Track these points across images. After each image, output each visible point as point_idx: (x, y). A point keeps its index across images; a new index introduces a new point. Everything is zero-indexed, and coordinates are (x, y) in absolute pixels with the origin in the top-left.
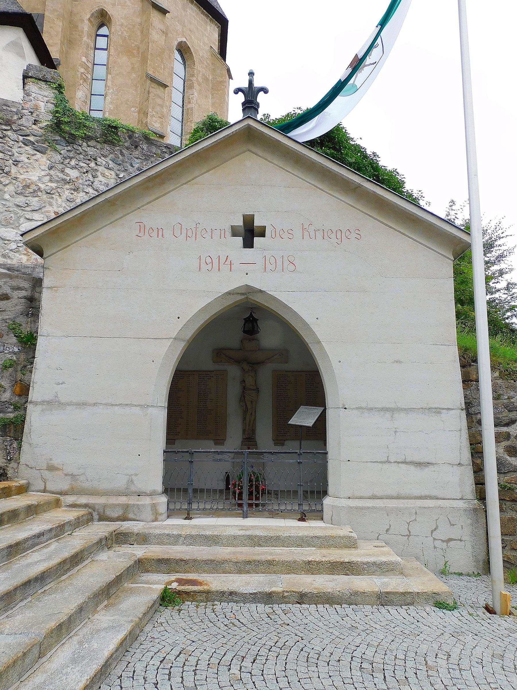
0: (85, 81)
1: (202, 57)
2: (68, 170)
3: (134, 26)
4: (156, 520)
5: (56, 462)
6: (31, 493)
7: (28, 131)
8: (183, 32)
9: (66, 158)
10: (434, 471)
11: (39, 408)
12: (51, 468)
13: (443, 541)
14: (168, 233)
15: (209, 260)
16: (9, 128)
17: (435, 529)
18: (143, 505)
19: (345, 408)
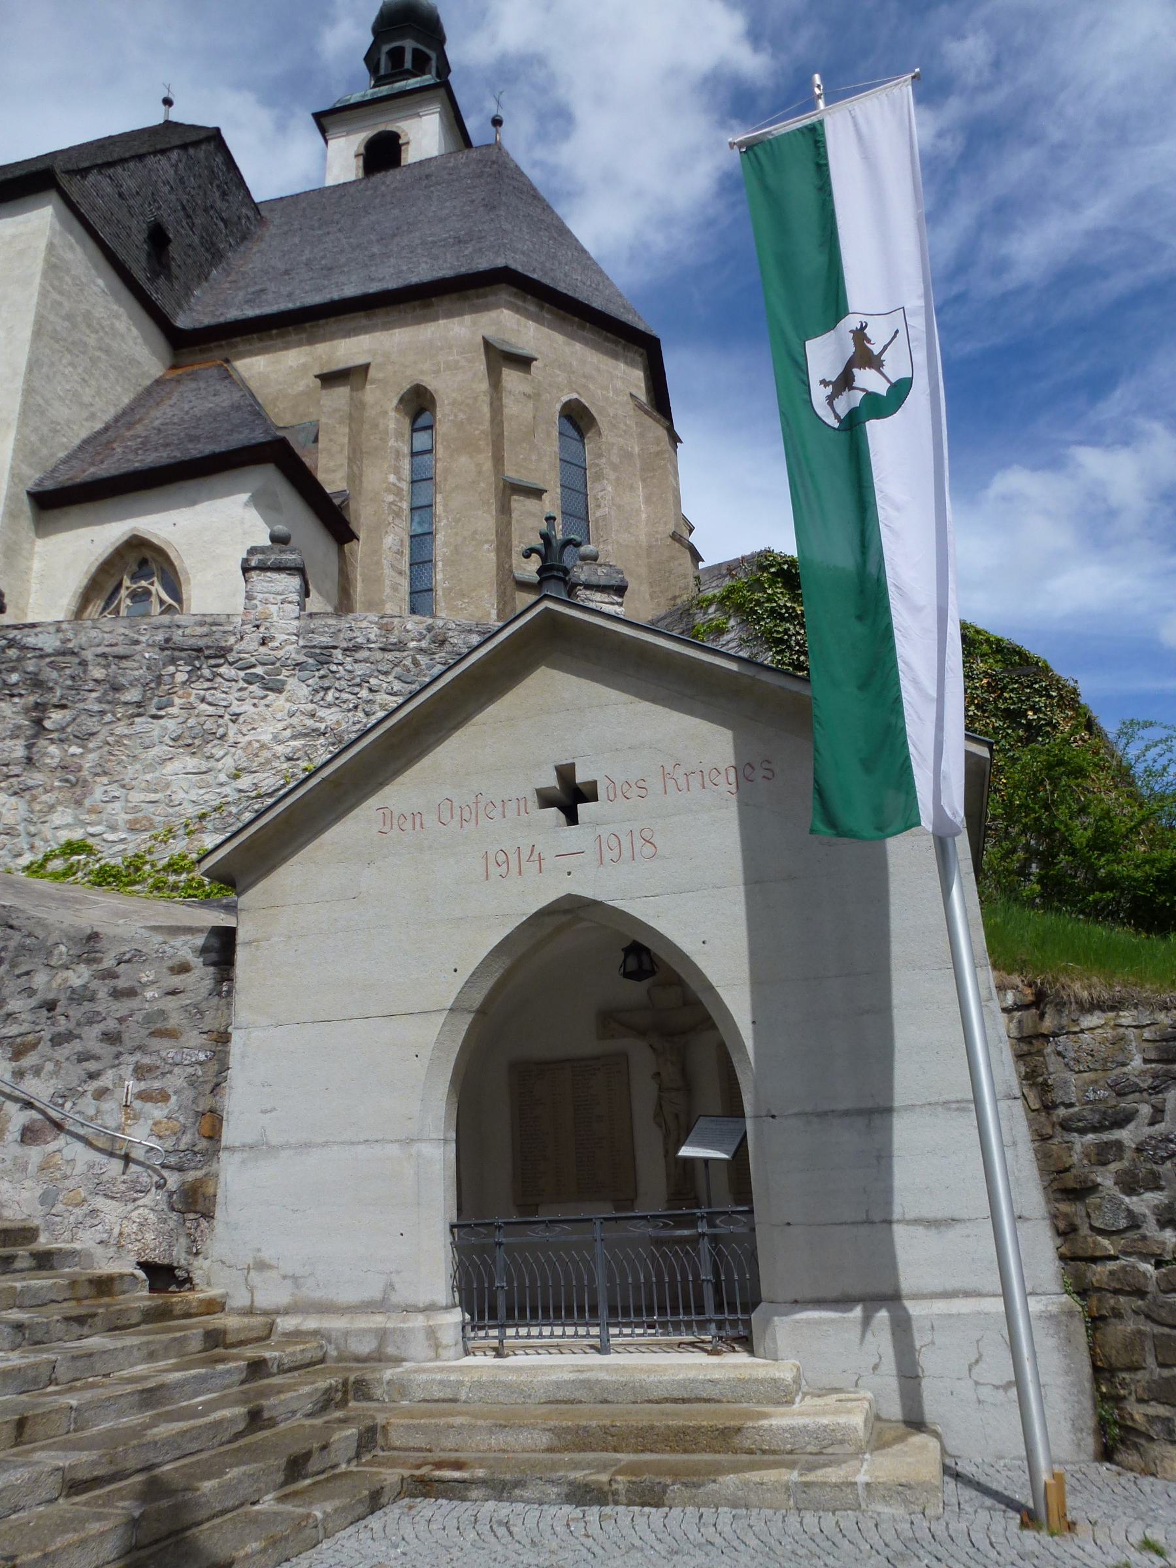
0: (398, 515)
1: (615, 416)
2: (322, 713)
3: (476, 398)
4: (437, 1357)
5: (267, 1255)
6: (122, 1297)
7: (253, 660)
8: (570, 382)
9: (317, 691)
10: (968, 1236)
11: (237, 1157)
12: (262, 1266)
13: (997, 1387)
14: (430, 820)
15: (501, 858)
16: (222, 661)
17: (977, 1361)
18: (411, 1330)
19: (773, 1117)
